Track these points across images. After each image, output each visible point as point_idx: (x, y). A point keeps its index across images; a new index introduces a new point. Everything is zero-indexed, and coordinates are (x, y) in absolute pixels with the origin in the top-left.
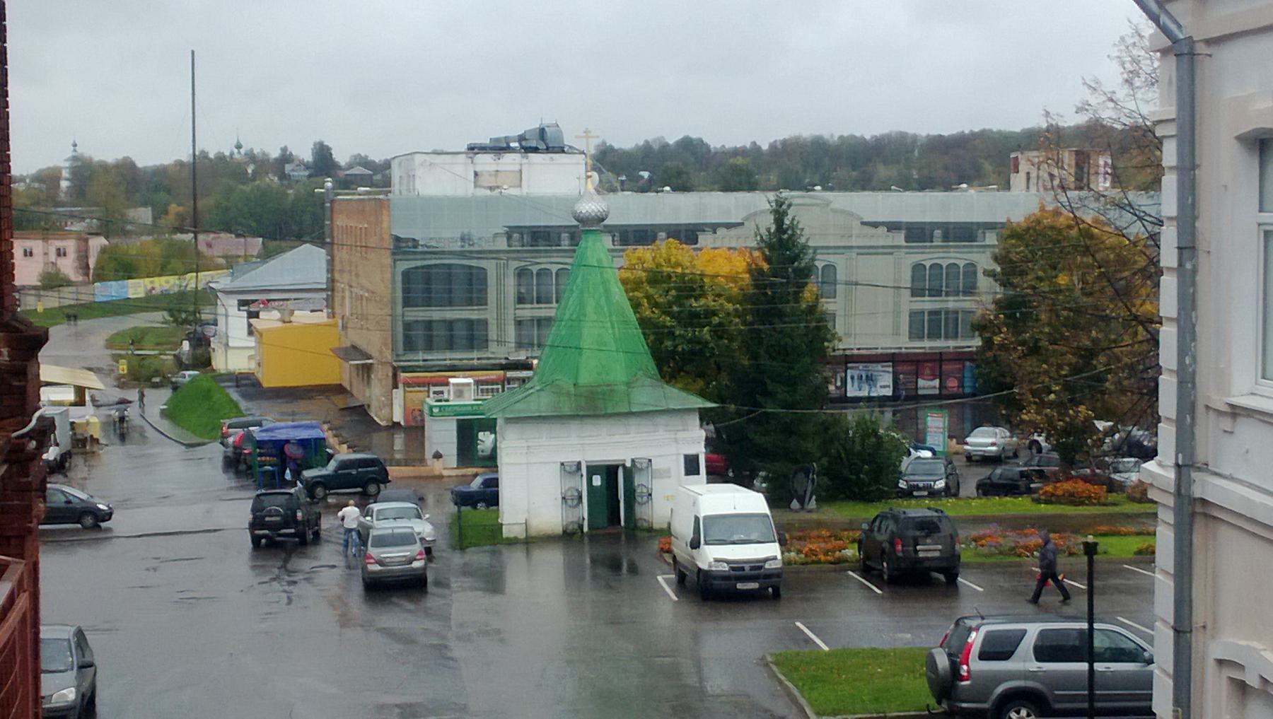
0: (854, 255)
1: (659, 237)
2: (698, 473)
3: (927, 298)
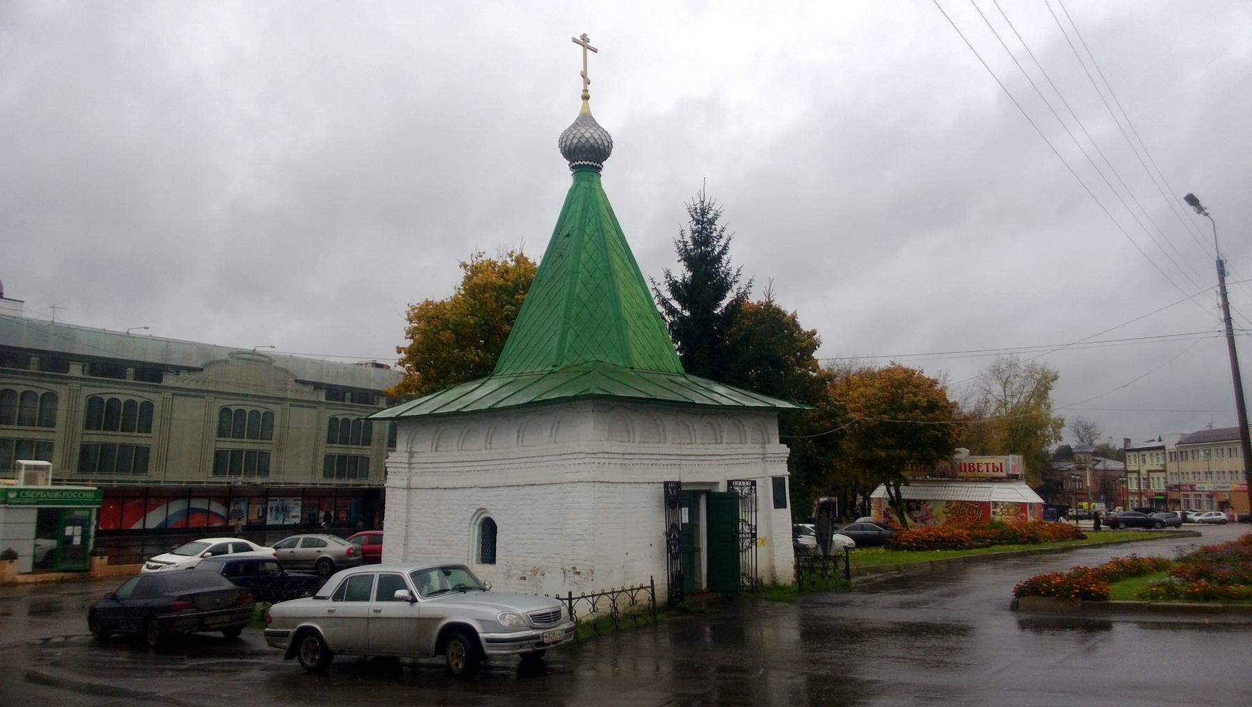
0: (288, 406)
1: (32, 362)
3: (337, 445)
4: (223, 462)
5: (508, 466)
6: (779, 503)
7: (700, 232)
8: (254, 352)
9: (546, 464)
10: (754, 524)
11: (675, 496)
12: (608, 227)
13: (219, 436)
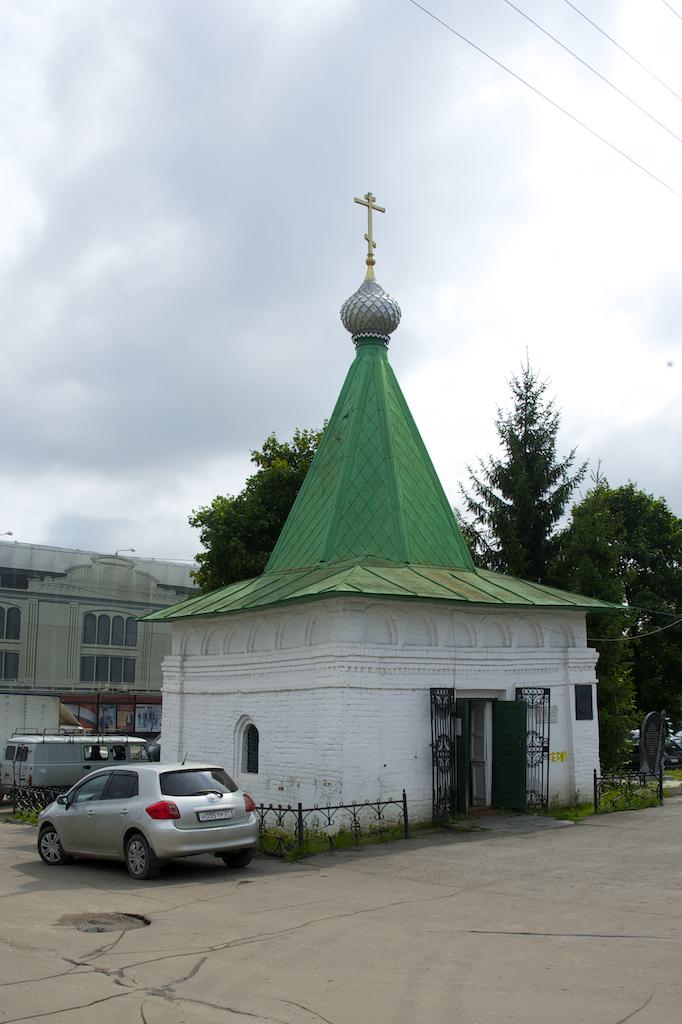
2: (590, 717)
4: (90, 668)
5: (267, 671)
6: (583, 713)
7: (525, 409)
8: (115, 557)
9: (300, 668)
10: (546, 736)
11: (446, 705)
12: (391, 406)
13: (84, 642)
